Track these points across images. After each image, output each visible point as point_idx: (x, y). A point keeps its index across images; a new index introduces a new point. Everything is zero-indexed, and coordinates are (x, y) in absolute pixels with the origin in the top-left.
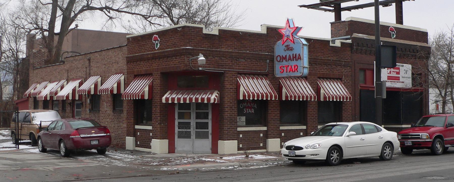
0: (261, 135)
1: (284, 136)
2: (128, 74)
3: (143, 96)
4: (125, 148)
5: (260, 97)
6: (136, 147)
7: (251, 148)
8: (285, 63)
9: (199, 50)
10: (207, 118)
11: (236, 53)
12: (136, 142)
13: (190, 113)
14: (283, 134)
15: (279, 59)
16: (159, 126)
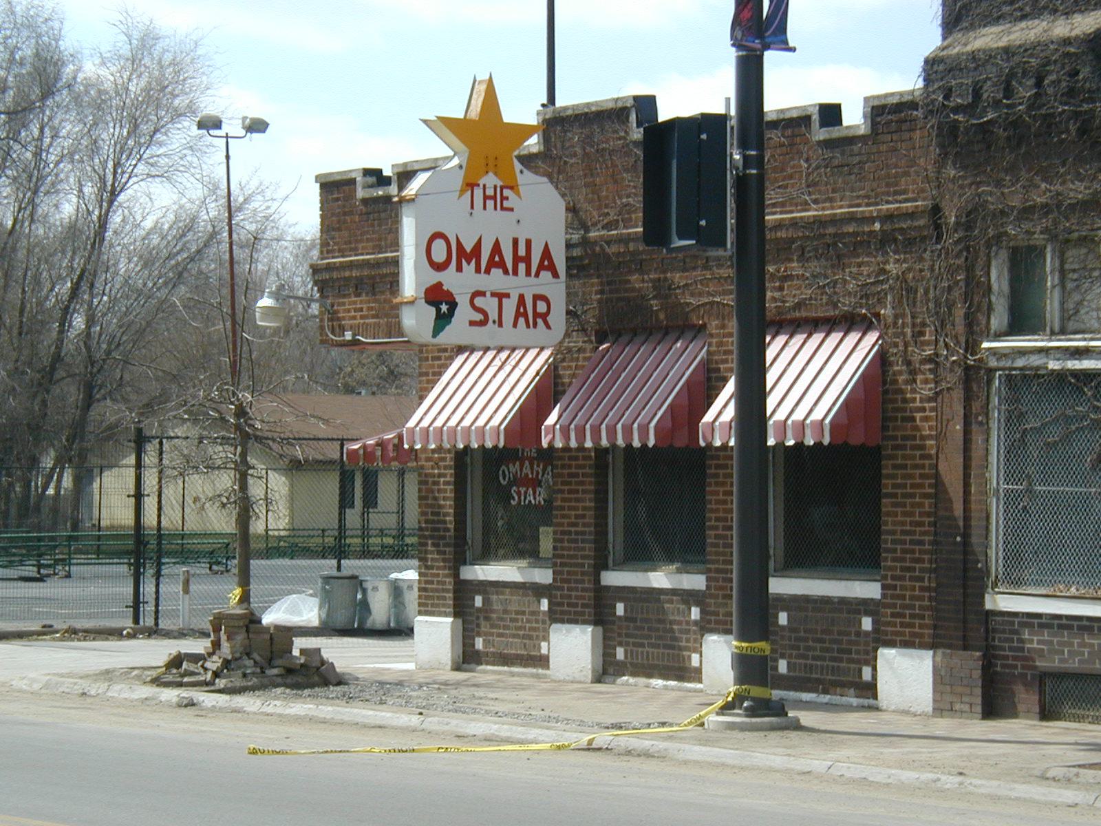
1: (790, 628)
7: (819, 681)
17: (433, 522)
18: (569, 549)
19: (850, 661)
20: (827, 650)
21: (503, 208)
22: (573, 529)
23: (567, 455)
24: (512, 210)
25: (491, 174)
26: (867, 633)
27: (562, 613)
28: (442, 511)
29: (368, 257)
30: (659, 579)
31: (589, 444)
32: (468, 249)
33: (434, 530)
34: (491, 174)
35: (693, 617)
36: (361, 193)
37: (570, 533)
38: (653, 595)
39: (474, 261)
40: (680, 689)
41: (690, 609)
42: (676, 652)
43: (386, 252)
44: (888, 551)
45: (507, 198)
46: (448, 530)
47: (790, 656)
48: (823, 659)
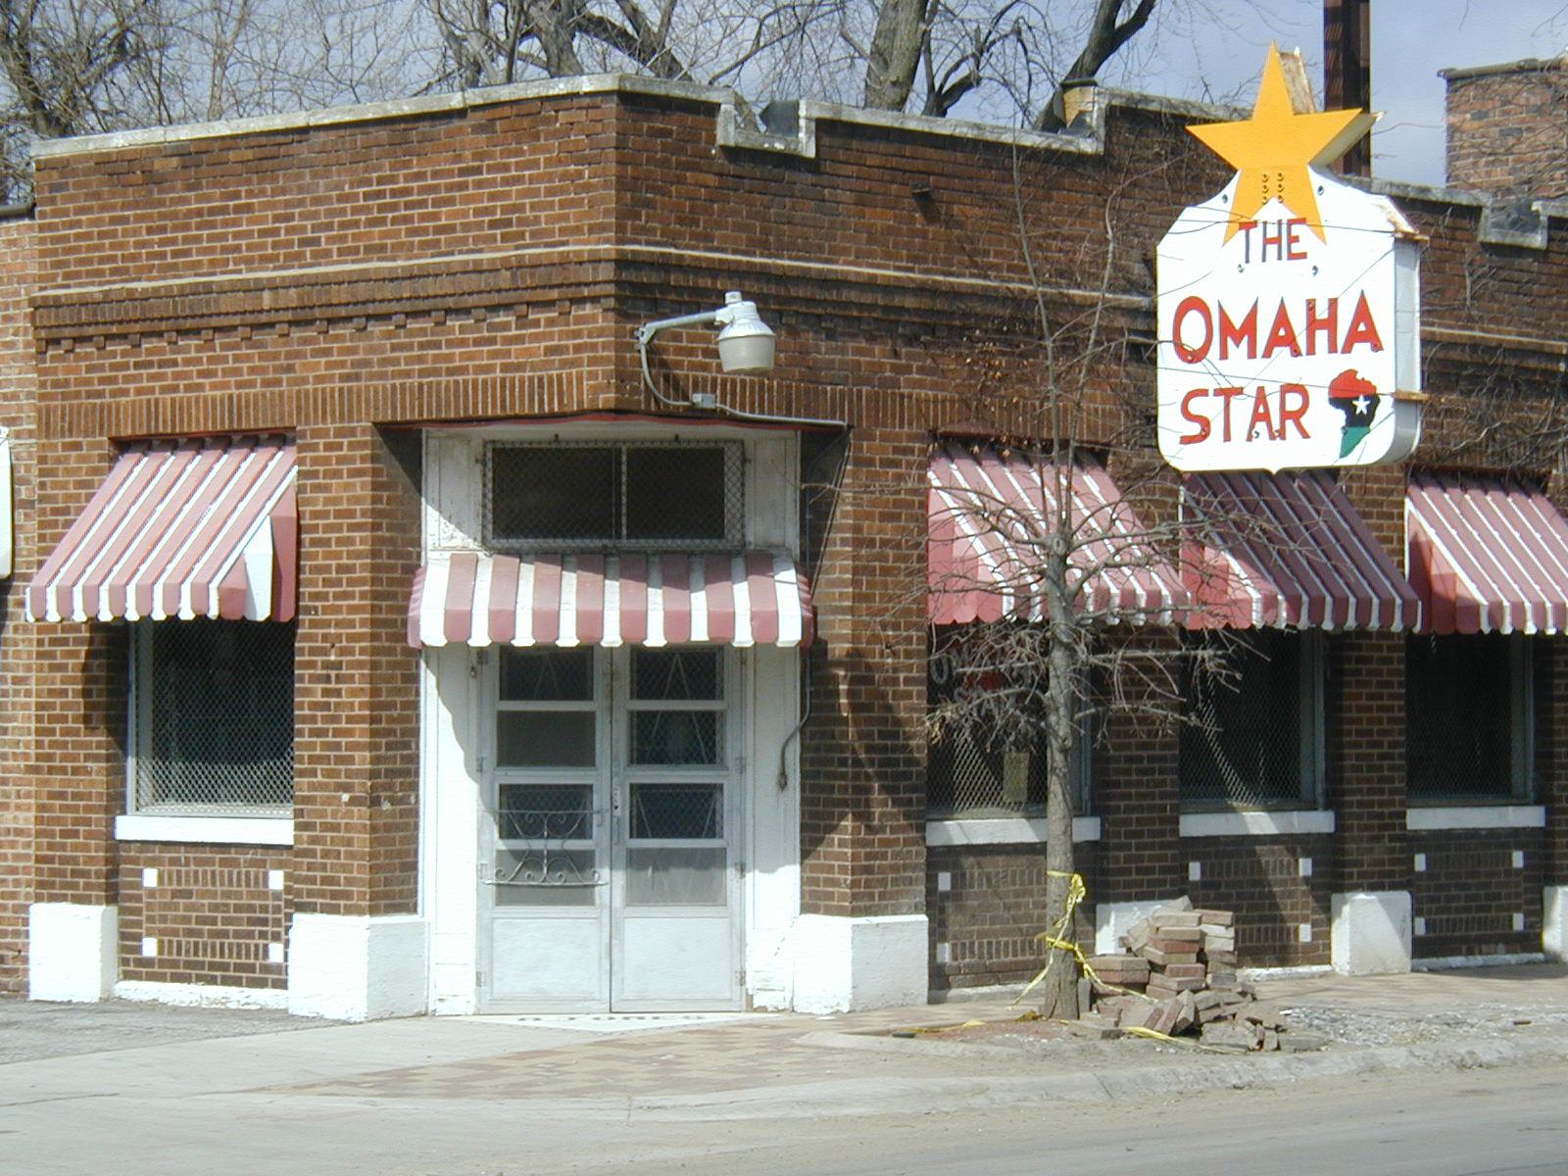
0: (1518, 859)
1: (1429, 874)
2: (46, 427)
3: (237, 595)
4: (23, 988)
5: (1508, 619)
6: (128, 976)
7: (1465, 940)
8: (1238, 366)
9: (716, 270)
10: (583, 756)
11: (921, 290)
12: (128, 939)
13: (588, 718)
14: (1420, 862)
15: (1193, 331)
16: (360, 815)
17: (884, 749)
18: (1139, 784)
19: (1500, 908)
20: (1474, 898)
21: (1292, 256)
22: (1145, 754)
23: (1385, 643)
24: (1303, 256)
25: (1274, 202)
26: (1518, 871)
27: (1127, 884)
28: (901, 730)
29: (738, 257)
30: (1259, 822)
31: (1397, 626)
32: (1237, 322)
33: (884, 763)
34: (1274, 202)
35: (1301, 873)
36: (727, 133)
37: (1140, 759)
38: (1248, 843)
39: (1246, 338)
40: (1291, 977)
41: (1297, 861)
42: (1278, 925)
43: (781, 257)
44: (304, 719)
45: (1296, 239)
46: (917, 762)
47: (1430, 912)
48: (1467, 910)
